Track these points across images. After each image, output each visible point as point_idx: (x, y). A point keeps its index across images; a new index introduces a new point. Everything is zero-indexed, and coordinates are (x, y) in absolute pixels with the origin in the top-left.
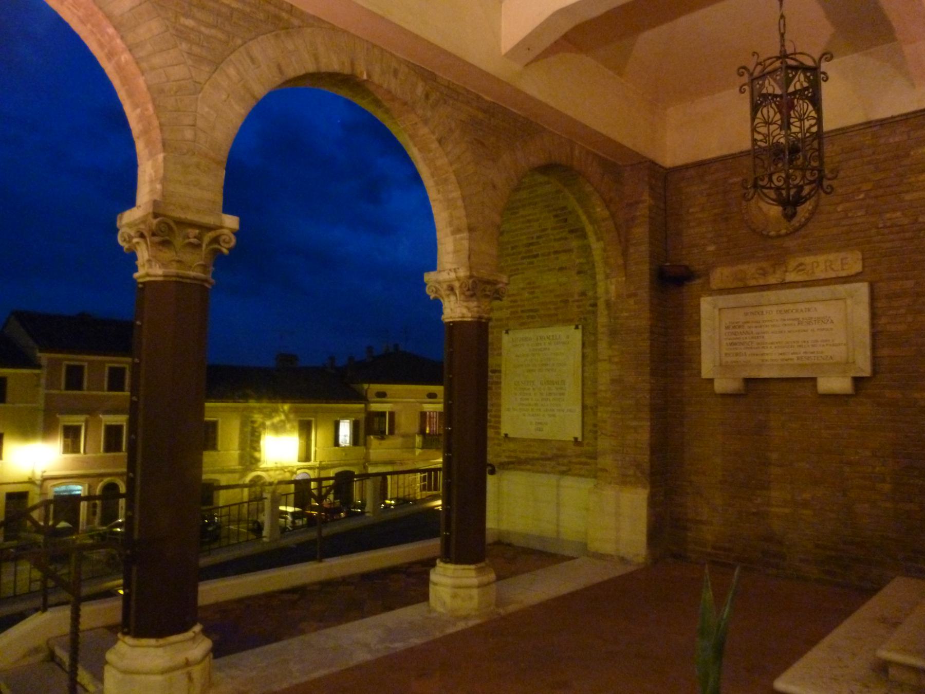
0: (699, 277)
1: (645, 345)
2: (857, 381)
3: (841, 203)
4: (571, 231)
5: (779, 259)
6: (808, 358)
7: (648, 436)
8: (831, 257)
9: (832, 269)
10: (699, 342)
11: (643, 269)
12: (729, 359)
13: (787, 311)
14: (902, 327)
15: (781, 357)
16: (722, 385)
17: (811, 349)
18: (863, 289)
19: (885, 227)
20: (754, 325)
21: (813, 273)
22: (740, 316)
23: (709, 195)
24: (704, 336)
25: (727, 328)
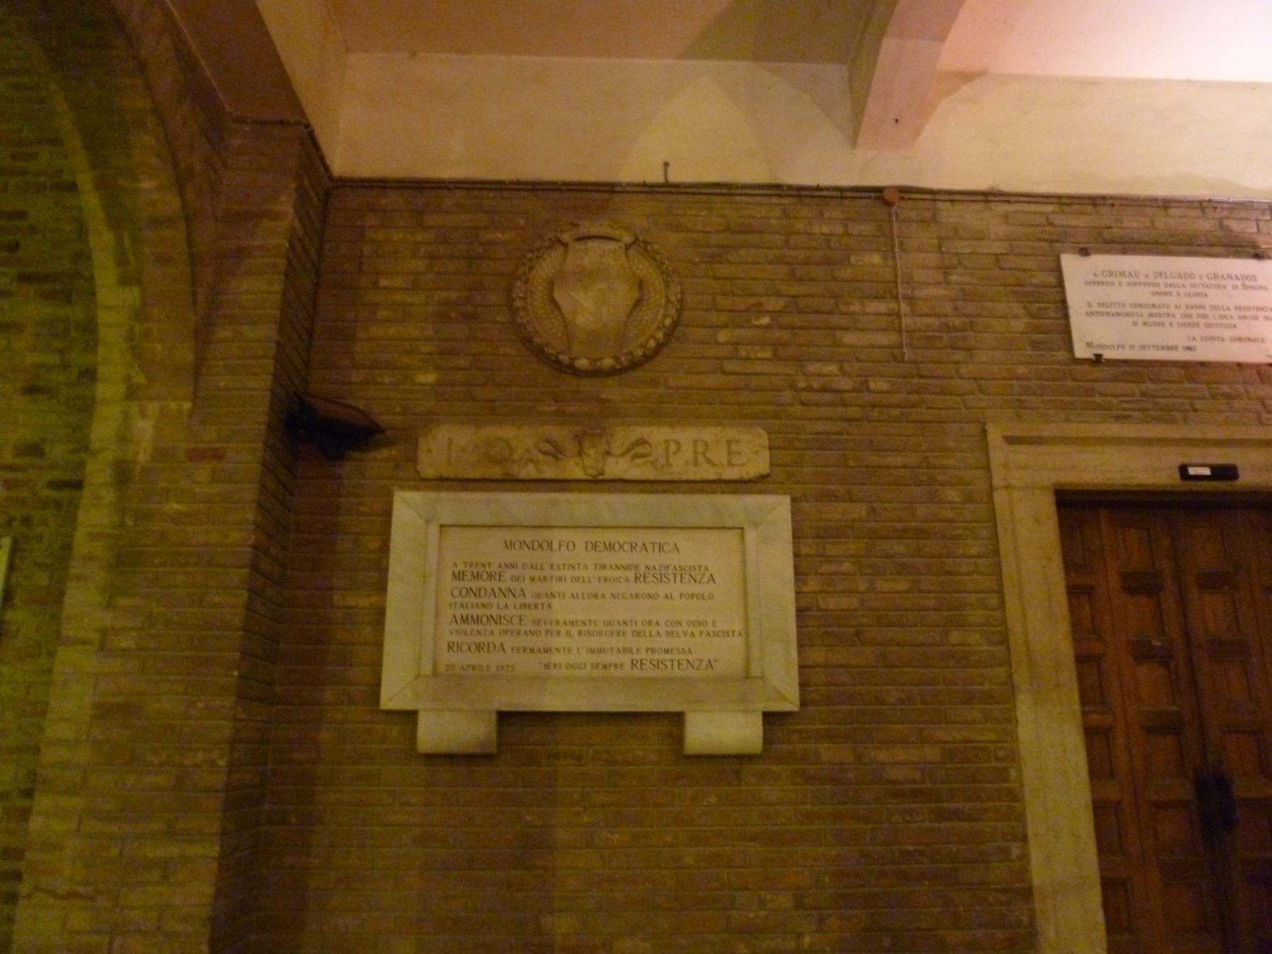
0: (389, 443)
1: (230, 604)
2: (770, 718)
3: (725, 326)
4: (24, 278)
5: (592, 425)
6: (657, 665)
7: (209, 890)
8: (708, 434)
9: (710, 462)
10: (380, 614)
11: (251, 391)
12: (457, 659)
13: (610, 547)
14: (845, 602)
15: (596, 658)
16: (440, 730)
17: (665, 642)
18: (778, 508)
19: (809, 389)
20: (528, 573)
21: (669, 464)
22: (492, 548)
23: (432, 257)
24: (396, 591)
25: (458, 576)
